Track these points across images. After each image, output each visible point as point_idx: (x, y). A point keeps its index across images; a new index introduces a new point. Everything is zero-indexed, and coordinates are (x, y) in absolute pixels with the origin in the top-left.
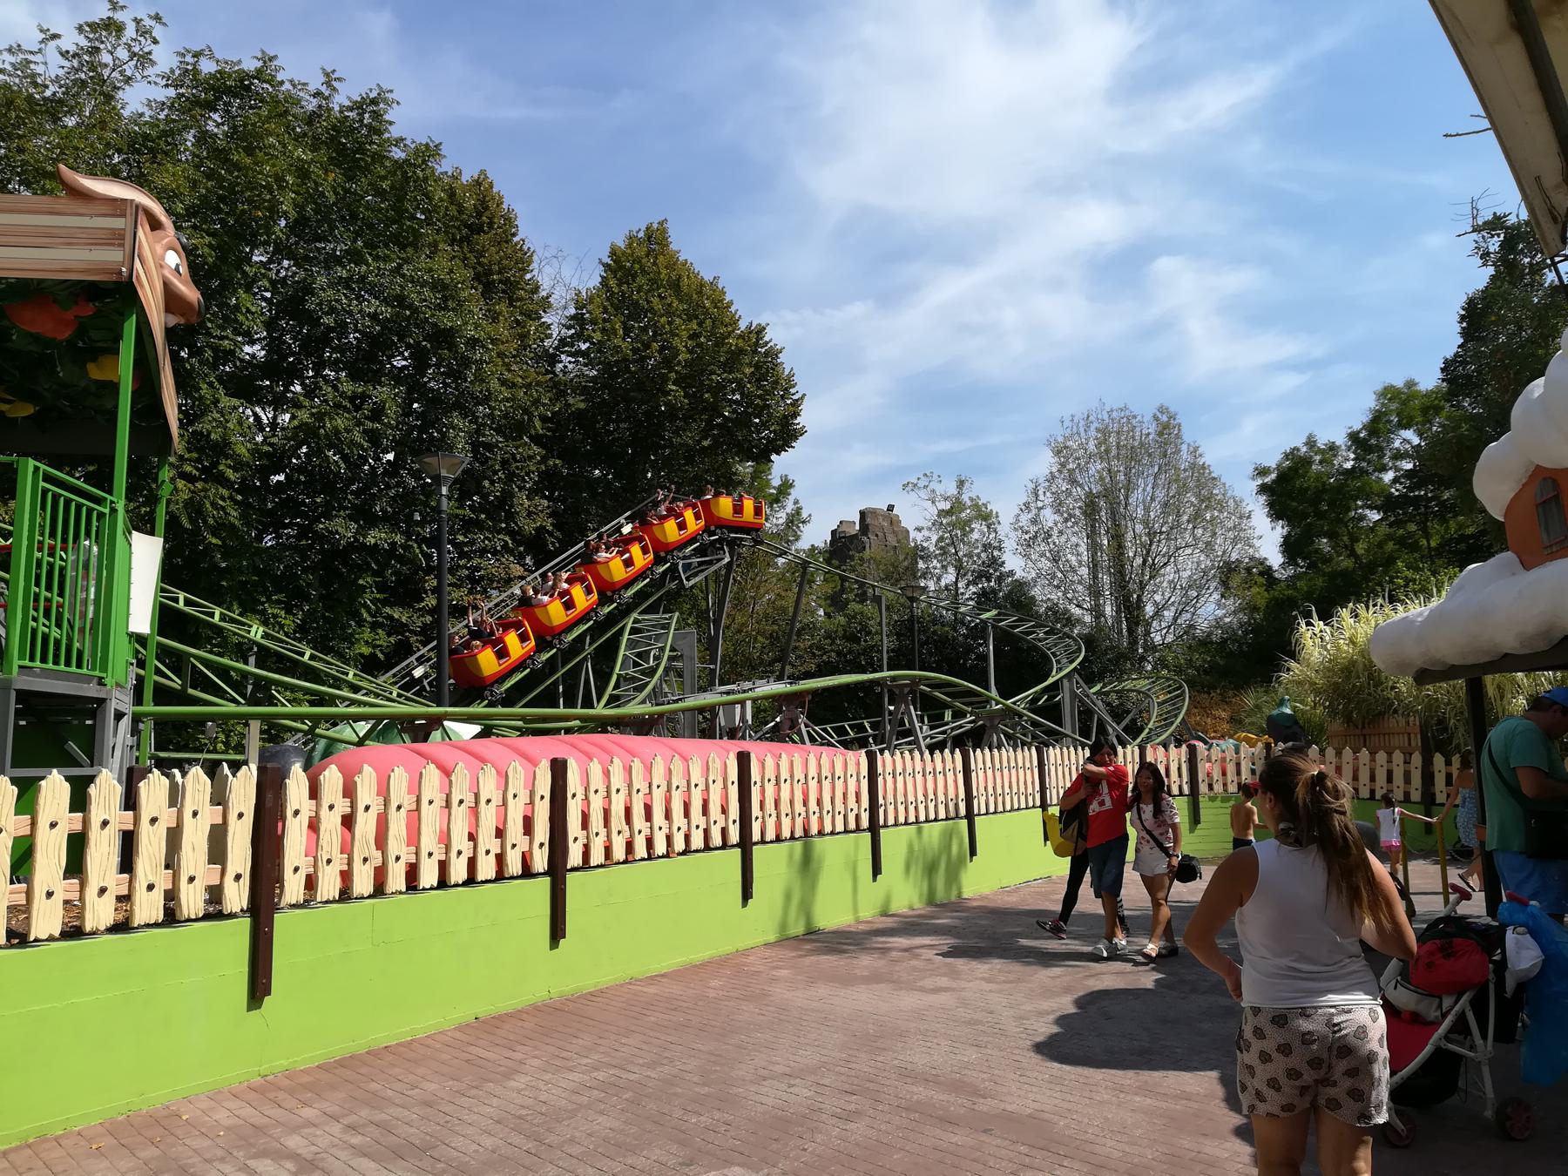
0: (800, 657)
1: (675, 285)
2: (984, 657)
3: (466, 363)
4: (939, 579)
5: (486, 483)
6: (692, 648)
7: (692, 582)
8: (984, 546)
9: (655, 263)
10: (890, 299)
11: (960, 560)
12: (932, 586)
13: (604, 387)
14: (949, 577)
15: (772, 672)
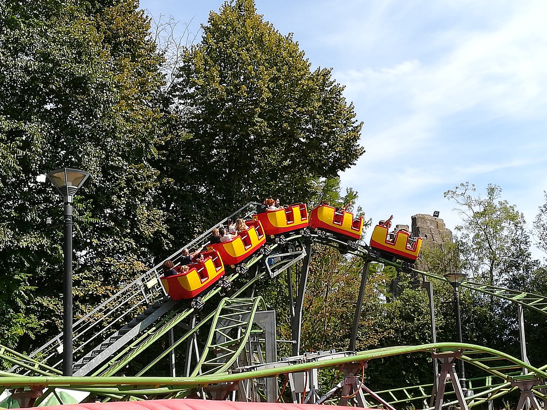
0: (365, 333)
1: (260, 41)
2: (516, 333)
3: (95, 103)
4: (477, 268)
5: (114, 198)
6: (272, 325)
7: (276, 273)
8: (513, 241)
9: (244, 26)
10: (430, 58)
11: (493, 253)
12: (471, 274)
13: (206, 121)
14: (485, 267)
15: (343, 346)
